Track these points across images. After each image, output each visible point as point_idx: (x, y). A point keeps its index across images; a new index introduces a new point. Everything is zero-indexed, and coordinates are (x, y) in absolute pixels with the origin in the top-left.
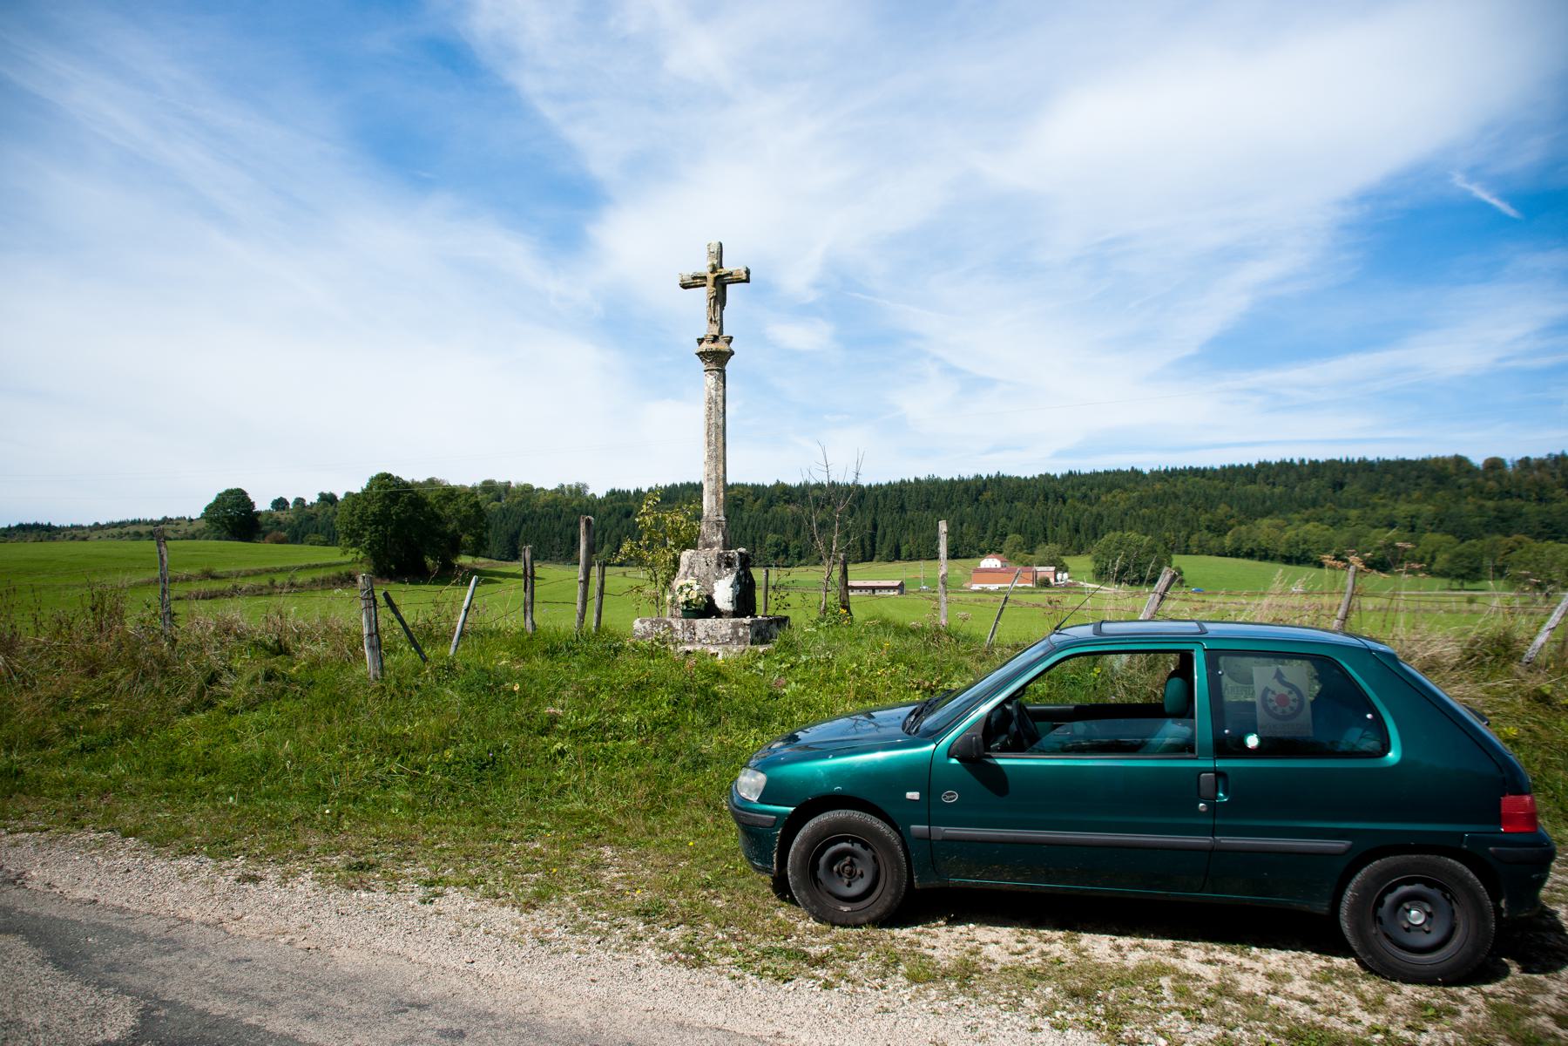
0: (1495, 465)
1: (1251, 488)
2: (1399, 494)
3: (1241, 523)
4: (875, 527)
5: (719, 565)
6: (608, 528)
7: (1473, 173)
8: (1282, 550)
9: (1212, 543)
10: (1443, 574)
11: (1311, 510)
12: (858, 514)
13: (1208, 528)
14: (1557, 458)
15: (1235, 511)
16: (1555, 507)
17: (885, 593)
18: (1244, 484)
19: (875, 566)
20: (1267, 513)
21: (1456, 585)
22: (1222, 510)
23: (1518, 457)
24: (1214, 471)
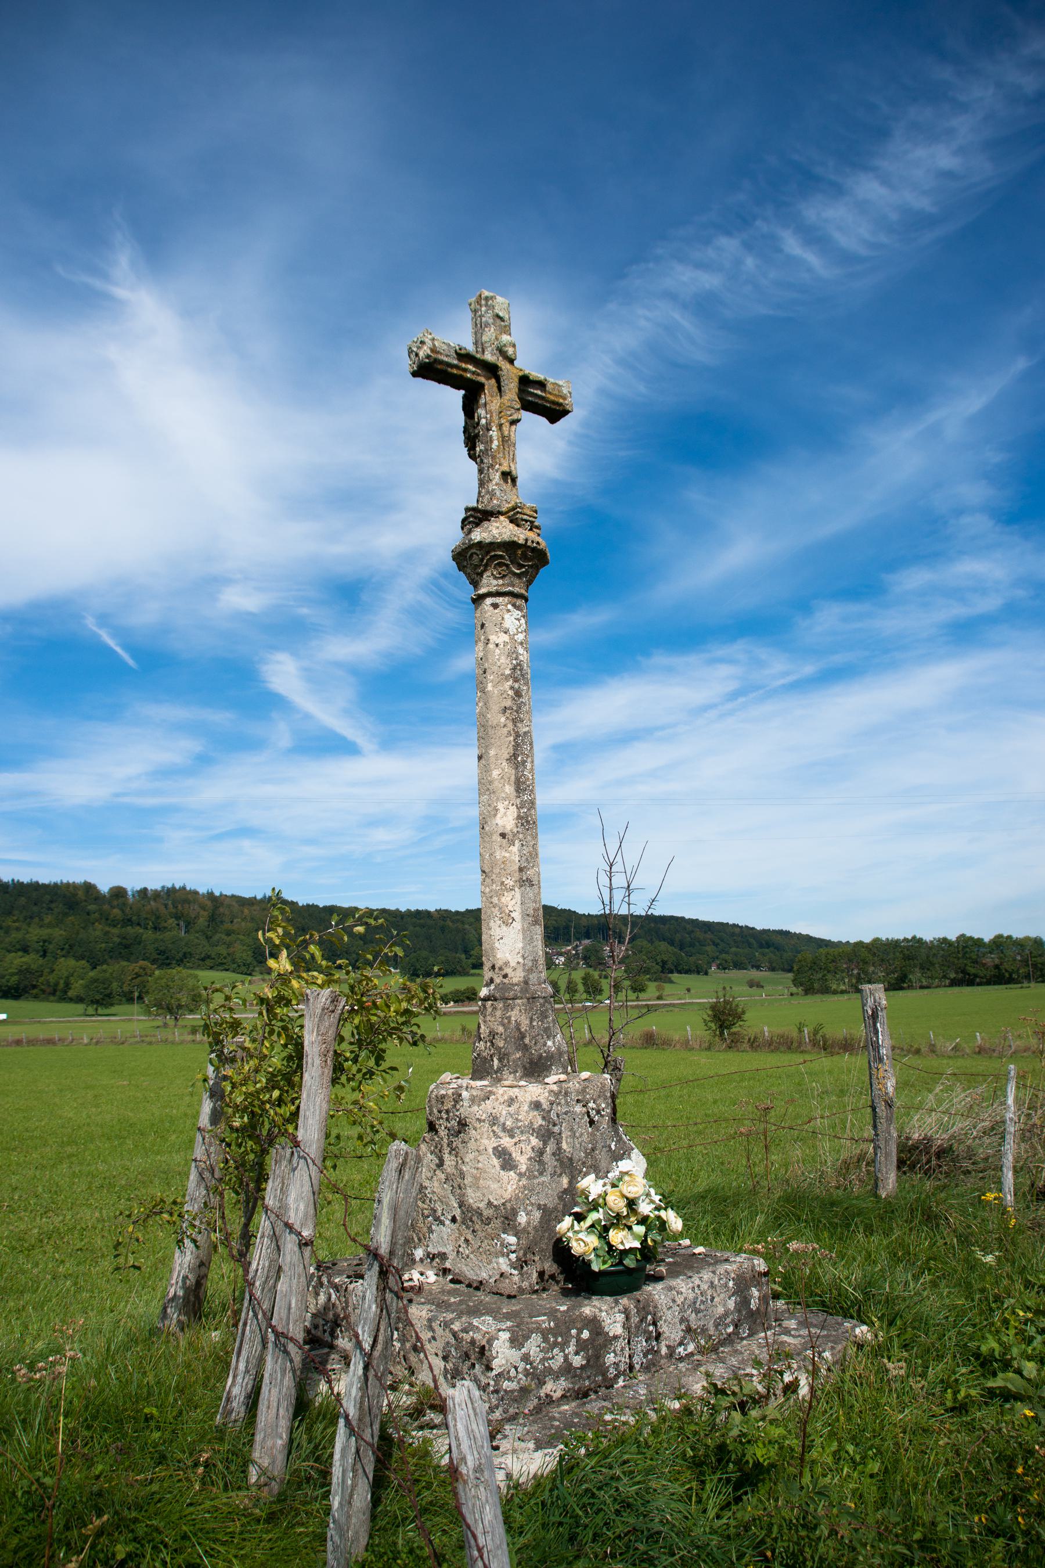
0: (118, 893)
2: (31, 918)
10: (79, 1000)
14: (168, 889)
21: (91, 1010)
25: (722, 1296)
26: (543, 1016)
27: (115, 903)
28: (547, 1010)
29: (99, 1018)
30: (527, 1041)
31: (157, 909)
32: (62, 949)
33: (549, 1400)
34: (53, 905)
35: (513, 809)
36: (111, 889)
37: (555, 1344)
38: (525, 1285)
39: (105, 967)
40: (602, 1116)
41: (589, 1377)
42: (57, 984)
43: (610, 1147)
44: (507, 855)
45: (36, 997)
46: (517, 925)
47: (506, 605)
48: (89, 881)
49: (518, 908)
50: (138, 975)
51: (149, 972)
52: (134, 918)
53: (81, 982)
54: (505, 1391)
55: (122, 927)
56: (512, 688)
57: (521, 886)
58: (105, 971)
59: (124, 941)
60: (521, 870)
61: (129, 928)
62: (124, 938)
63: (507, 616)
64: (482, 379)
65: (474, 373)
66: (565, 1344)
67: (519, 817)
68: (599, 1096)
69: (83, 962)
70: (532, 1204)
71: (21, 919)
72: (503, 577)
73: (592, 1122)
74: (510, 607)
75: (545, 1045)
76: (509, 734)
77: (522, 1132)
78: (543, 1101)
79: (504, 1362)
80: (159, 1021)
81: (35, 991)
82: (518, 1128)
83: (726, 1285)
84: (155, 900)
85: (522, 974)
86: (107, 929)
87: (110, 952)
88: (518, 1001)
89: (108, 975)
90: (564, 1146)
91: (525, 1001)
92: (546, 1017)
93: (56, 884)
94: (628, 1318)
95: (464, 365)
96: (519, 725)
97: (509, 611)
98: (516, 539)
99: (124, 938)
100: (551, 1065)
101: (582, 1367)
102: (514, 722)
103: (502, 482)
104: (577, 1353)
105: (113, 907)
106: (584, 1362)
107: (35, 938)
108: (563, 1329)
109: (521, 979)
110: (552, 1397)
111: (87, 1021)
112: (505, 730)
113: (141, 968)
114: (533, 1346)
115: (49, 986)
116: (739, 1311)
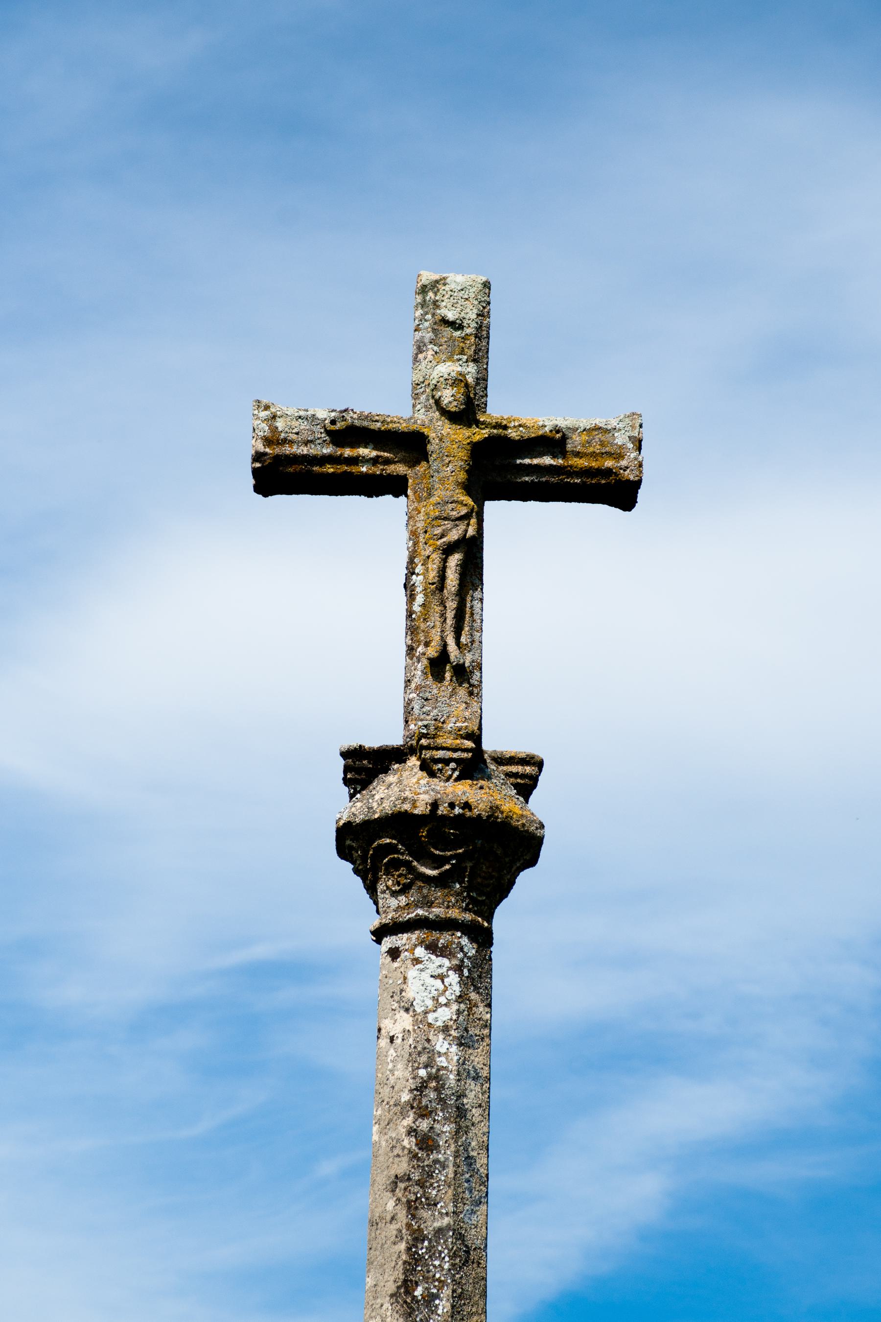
56: (411, 1131)
64: (400, 469)
65: (375, 461)
72: (405, 890)
74: (420, 952)
76: (399, 1236)
95: (347, 452)
96: (425, 1214)
97: (417, 961)
98: (407, 807)
102: (412, 1207)
103: (430, 681)
112: (393, 1228)
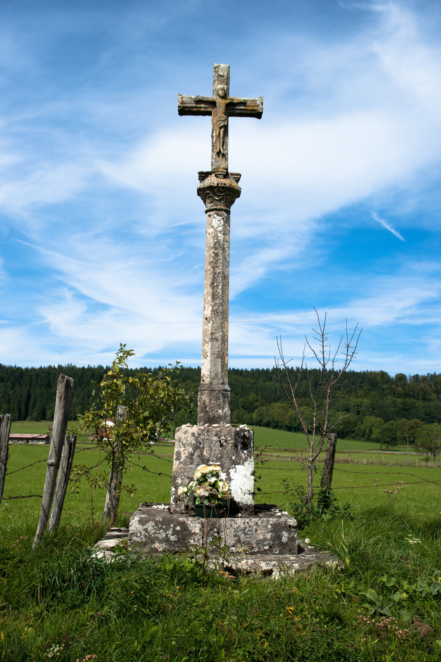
0: (401, 377)
1: (268, 383)
2: (351, 392)
3: (262, 405)
4: (29, 397)
5: (236, 446)
6: (157, 399)
7: (382, 213)
8: (287, 422)
9: (245, 416)
10: (377, 441)
11: (303, 399)
12: (17, 387)
13: (243, 407)
14: (432, 375)
15: (259, 397)
16: (431, 404)
17: (35, 442)
18: (265, 381)
19: (27, 424)
20: (277, 399)
21: (384, 447)
22: (252, 396)
23: (413, 374)
24: (246, 371)
25: (263, 531)
26: (217, 399)
27: (399, 383)
28: (219, 396)
29: (389, 452)
30: (208, 409)
31: (425, 388)
32: (368, 411)
33: (156, 550)
34: (363, 385)
35: (211, 307)
36: (397, 375)
37: (162, 528)
38: (178, 509)
39: (392, 422)
40: (228, 443)
41: (178, 547)
42: (365, 431)
43: (231, 458)
44: (207, 327)
45: (353, 438)
46: (209, 358)
47: (213, 215)
48: (383, 370)
49: (209, 351)
50: (412, 428)
51: (419, 426)
52: (411, 393)
53: (378, 430)
54: (134, 541)
55: (403, 398)
57: (211, 341)
58: (393, 424)
59: (405, 407)
60: (212, 334)
61: (408, 399)
62: (405, 405)
63: (213, 220)
66: (167, 529)
67: (213, 310)
68: (228, 434)
69: (379, 418)
70: (184, 476)
71: (345, 392)
73: (221, 445)
74: (215, 215)
75: (217, 411)
76: (211, 273)
77: (188, 446)
78: (195, 433)
79: (135, 529)
80: (424, 456)
81: (353, 435)
82: (187, 444)
83: (266, 526)
84: (423, 382)
85: (209, 380)
86: (394, 399)
87: (397, 413)
88: (206, 391)
89: (394, 427)
90: (205, 453)
91: (208, 391)
92: (219, 399)
93: (364, 372)
94: (203, 527)
96: (216, 269)
97: (214, 217)
99: (405, 405)
100: (220, 421)
101: (175, 541)
102: (214, 268)
104: (173, 535)
105: (398, 386)
106: (176, 540)
107: (353, 404)
108: (167, 523)
109: (209, 382)
110: (158, 550)
111: (382, 454)
112: (210, 272)
113: (414, 423)
114: (150, 526)
115: (361, 432)
116: (274, 541)
